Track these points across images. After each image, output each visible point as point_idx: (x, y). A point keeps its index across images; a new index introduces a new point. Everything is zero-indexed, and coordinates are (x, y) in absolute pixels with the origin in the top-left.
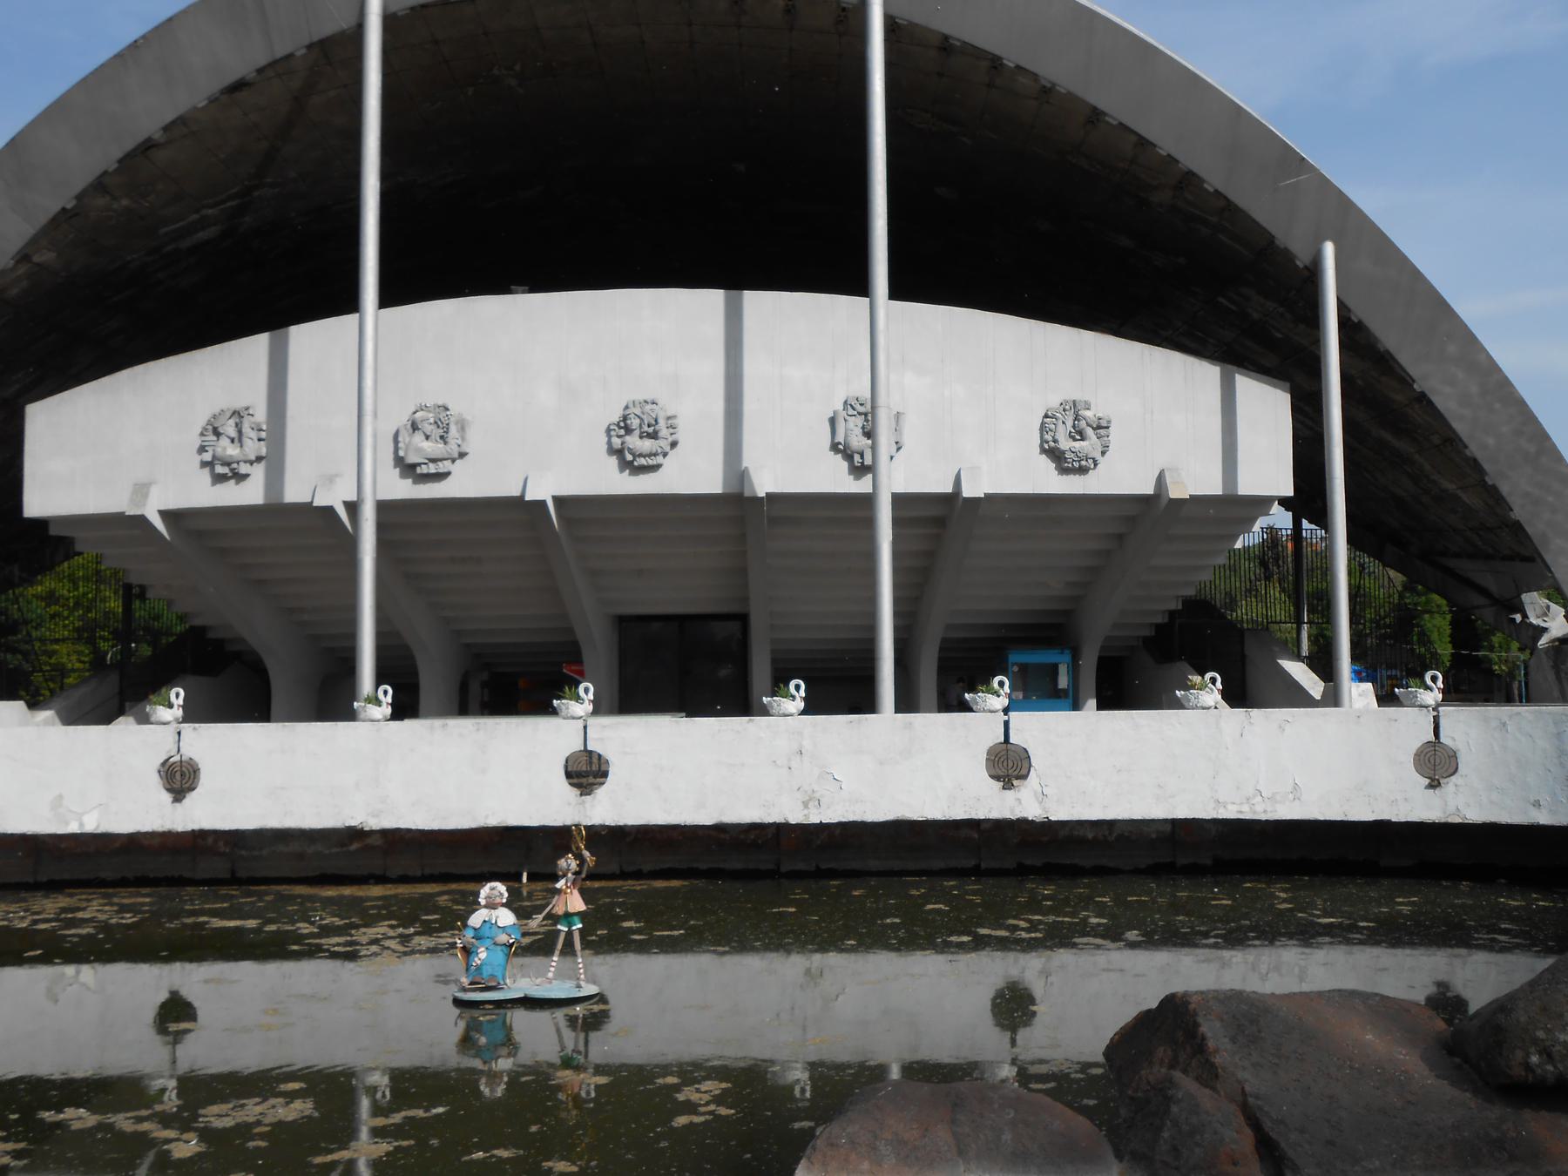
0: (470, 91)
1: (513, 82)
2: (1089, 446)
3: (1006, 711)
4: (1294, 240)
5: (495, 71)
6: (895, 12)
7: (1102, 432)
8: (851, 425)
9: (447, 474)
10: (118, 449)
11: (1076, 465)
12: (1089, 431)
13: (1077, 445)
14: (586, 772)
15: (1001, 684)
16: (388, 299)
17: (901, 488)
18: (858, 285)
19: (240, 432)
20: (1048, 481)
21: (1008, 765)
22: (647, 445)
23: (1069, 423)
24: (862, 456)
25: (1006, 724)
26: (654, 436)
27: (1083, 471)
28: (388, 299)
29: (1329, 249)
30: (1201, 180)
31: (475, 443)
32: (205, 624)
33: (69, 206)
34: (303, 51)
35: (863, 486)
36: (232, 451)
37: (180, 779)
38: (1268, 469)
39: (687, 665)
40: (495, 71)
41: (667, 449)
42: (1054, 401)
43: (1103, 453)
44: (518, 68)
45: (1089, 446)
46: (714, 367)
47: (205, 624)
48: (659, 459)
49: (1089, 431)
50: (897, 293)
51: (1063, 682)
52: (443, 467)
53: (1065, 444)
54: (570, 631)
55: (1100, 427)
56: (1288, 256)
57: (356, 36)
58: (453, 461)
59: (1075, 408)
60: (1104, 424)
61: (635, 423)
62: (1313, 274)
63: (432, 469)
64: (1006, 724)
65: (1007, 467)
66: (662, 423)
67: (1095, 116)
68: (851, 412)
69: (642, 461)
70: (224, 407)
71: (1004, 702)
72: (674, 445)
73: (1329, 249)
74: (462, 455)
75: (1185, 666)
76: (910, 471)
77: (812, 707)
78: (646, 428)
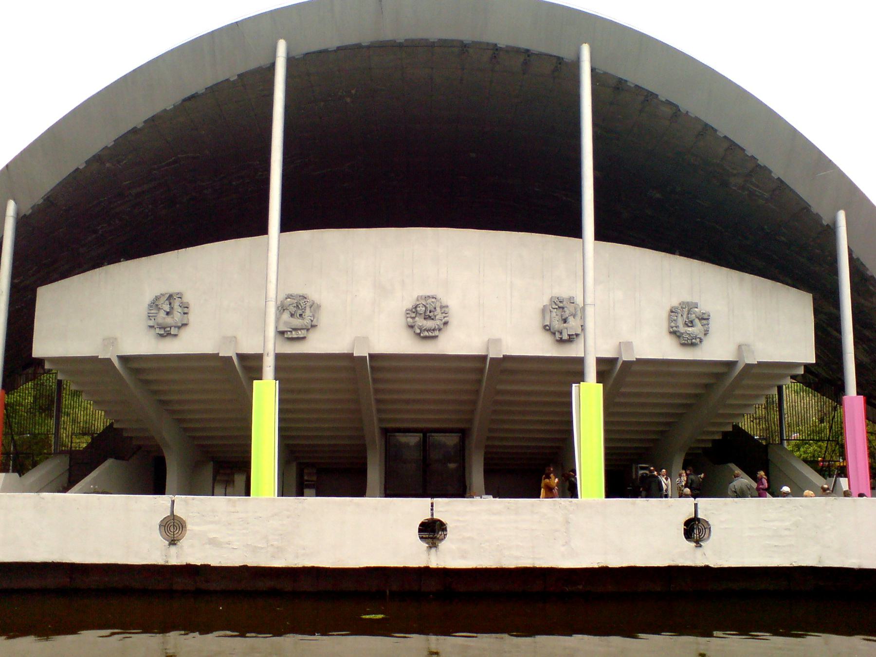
0: (322, 104)
1: (348, 100)
2: (697, 329)
4: (819, 207)
7: (705, 322)
8: (554, 314)
9: (304, 338)
10: (98, 318)
11: (689, 342)
16: (286, 226)
17: (608, 353)
18: (576, 231)
19: (172, 308)
20: (668, 350)
21: (173, 528)
22: (429, 324)
23: (685, 316)
24: (561, 333)
25: (696, 505)
26: (427, 318)
27: (693, 345)
28: (286, 226)
29: (842, 217)
30: (770, 172)
31: (324, 320)
32: (169, 431)
33: (81, 167)
34: (236, 78)
36: (169, 320)
37: (173, 528)
38: (802, 350)
39: (427, 468)
41: (442, 326)
42: (675, 303)
43: (705, 334)
45: (697, 329)
46: (580, 285)
47: (169, 431)
48: (437, 333)
49: (697, 321)
50: (600, 235)
52: (301, 334)
53: (682, 329)
54: (363, 437)
56: (817, 219)
57: (271, 68)
58: (308, 330)
59: (689, 307)
60: (705, 316)
61: (421, 309)
62: (831, 231)
64: (696, 505)
65: (653, 344)
66: (438, 309)
68: (554, 306)
69: (426, 334)
70: (163, 292)
72: (446, 323)
73: (842, 217)
74: (313, 326)
75: (733, 466)
76: (594, 347)
78: (428, 313)
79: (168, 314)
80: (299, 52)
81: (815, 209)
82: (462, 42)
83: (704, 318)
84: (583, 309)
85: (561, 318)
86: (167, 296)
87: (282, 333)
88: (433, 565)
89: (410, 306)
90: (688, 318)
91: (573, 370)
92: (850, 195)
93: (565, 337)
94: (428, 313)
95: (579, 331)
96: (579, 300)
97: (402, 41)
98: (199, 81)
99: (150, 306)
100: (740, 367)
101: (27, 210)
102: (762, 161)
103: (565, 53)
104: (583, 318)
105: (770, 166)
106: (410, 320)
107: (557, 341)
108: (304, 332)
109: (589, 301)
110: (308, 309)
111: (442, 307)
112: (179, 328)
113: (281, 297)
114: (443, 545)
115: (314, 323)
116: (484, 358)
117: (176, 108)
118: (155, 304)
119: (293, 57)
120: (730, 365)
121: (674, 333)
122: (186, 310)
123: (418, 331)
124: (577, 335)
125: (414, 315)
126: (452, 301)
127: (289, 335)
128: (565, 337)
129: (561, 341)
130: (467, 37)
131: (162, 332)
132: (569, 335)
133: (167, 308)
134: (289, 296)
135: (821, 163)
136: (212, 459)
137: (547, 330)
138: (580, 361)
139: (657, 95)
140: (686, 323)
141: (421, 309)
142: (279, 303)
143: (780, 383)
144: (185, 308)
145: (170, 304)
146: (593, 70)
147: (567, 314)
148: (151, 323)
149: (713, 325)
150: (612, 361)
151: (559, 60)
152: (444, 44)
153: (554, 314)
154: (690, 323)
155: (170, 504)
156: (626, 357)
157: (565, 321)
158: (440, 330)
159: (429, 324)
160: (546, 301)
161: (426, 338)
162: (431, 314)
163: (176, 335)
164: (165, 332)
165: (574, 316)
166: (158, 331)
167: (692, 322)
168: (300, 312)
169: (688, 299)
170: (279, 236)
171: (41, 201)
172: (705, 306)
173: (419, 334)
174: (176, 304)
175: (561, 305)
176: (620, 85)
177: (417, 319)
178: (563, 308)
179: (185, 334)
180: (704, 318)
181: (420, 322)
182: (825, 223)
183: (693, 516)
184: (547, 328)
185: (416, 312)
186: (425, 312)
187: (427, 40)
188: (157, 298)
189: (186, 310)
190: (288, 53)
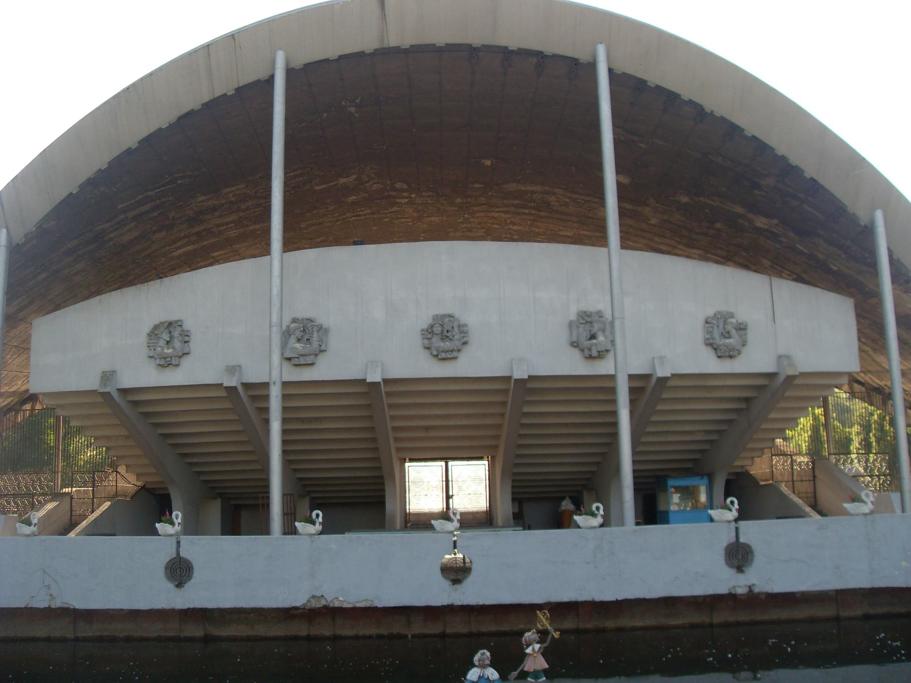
0: (325, 115)
1: (353, 110)
3: (736, 520)
5: (343, 103)
6: (612, 67)
7: (742, 332)
8: (581, 329)
10: (96, 345)
12: (733, 332)
13: (727, 341)
14: (179, 571)
15: (318, 515)
16: (289, 245)
17: (638, 368)
18: (599, 238)
19: (172, 337)
20: (710, 364)
22: (448, 345)
23: (721, 327)
24: (590, 350)
25: (737, 529)
26: (444, 338)
28: (289, 245)
30: (803, 171)
35: (604, 367)
40: (343, 103)
42: (710, 312)
43: (744, 345)
44: (358, 101)
46: (608, 298)
48: (455, 354)
49: (733, 332)
51: (703, 498)
52: (309, 360)
53: (719, 341)
55: (741, 329)
56: (853, 219)
57: (270, 81)
58: (316, 355)
60: (742, 326)
61: (437, 329)
62: (869, 231)
63: (302, 361)
64: (737, 529)
66: (456, 329)
67: (733, 130)
69: (443, 355)
70: (163, 320)
71: (734, 514)
73: (879, 216)
77: (327, 530)
79: (169, 340)
80: (299, 61)
81: (851, 208)
82: (470, 45)
83: (742, 328)
84: (612, 323)
85: (590, 333)
86: (166, 325)
87: (289, 359)
88: (458, 602)
89: (425, 326)
90: (725, 328)
91: (604, 387)
92: (886, 193)
93: (594, 353)
94: (445, 333)
95: (609, 347)
96: (608, 315)
97: (408, 47)
98: (194, 97)
99: (149, 335)
100: (782, 378)
101: (19, 237)
102: (794, 160)
103: (583, 56)
104: (613, 333)
105: (802, 166)
106: (426, 341)
107: (586, 358)
108: (312, 357)
109: (617, 315)
110: (315, 335)
111: (459, 326)
112: (180, 357)
113: (286, 321)
114: (188, 585)
115: (323, 348)
116: (507, 379)
117: (171, 126)
118: (154, 333)
119: (293, 69)
120: (771, 376)
121: (709, 343)
122: (187, 339)
123: (435, 353)
124: (607, 351)
125: (429, 336)
126: (471, 319)
127: (296, 361)
128: (594, 353)
129: (590, 357)
130: (476, 38)
131: (162, 362)
132: (599, 352)
133: (166, 337)
134: (294, 321)
135: (854, 163)
136: (221, 495)
137: (575, 347)
138: (612, 378)
139: (679, 95)
140: (723, 334)
141: (437, 329)
142: (284, 328)
143: (824, 393)
144: (186, 337)
145: (170, 332)
146: (610, 71)
147: (595, 330)
148: (151, 354)
149: (751, 335)
150: (646, 377)
151: (575, 62)
152: (452, 48)
153: (581, 329)
154: (726, 335)
155: (175, 546)
156: (660, 373)
157: (593, 337)
158: (459, 351)
159: (448, 345)
160: (573, 317)
161: (444, 359)
162: (448, 335)
163: (177, 365)
164: (167, 363)
165: (603, 331)
166: (158, 362)
167: (728, 332)
168: (307, 337)
169: (724, 308)
170: (282, 257)
171: (34, 229)
172: (743, 313)
173: (436, 356)
174: (176, 334)
175: (589, 320)
176: (640, 85)
177: (434, 340)
178: (591, 323)
179: (185, 362)
180: (742, 328)
181: (437, 343)
182: (862, 224)
183: (733, 540)
184: (574, 344)
185: (432, 333)
186: (442, 331)
187: (434, 45)
188: (156, 327)
189: (187, 339)
190: (287, 64)
